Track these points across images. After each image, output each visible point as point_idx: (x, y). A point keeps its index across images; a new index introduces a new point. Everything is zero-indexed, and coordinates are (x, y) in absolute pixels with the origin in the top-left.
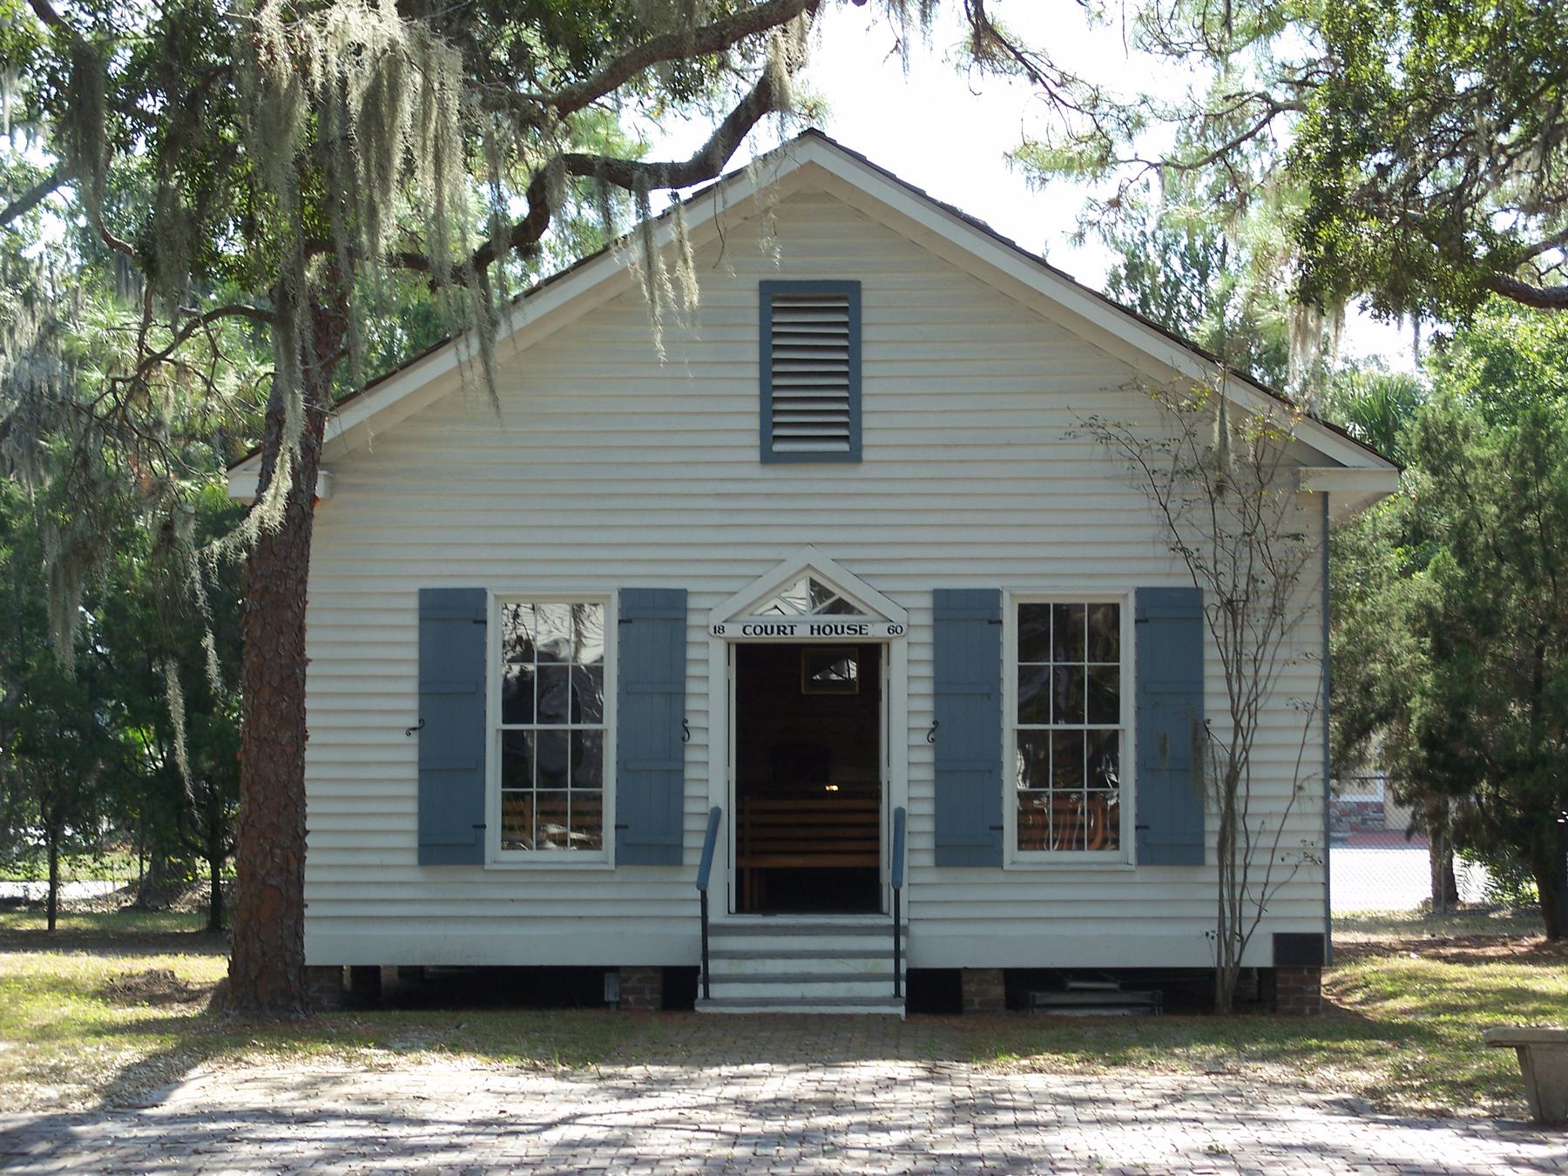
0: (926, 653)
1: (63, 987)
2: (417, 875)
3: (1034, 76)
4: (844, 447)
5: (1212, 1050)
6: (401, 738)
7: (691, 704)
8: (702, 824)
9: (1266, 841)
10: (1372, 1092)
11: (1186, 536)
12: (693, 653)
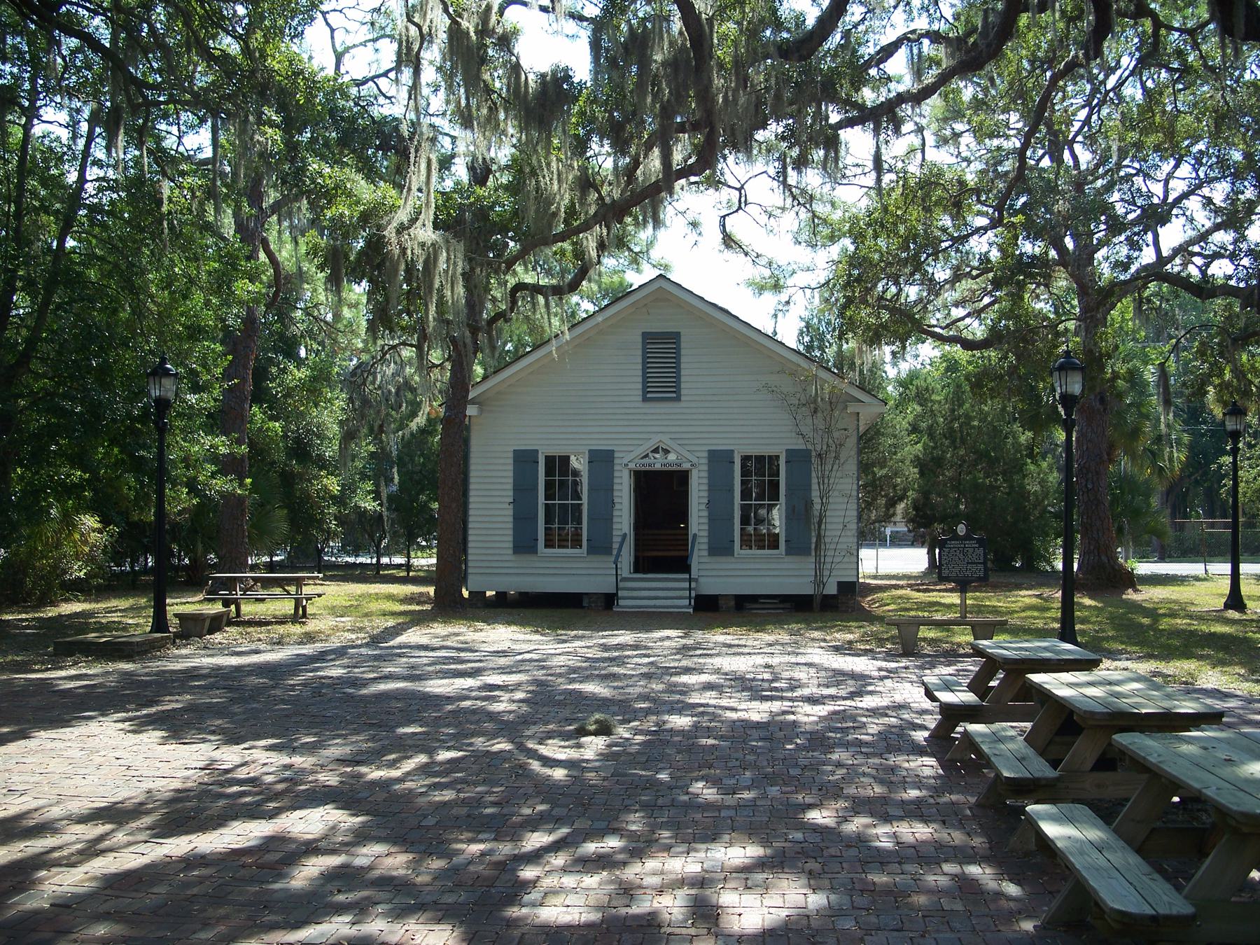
0: (705, 474)
1: (390, 597)
2: (513, 558)
3: (746, 254)
4: (674, 395)
5: (795, 626)
6: (507, 506)
7: (616, 494)
8: (619, 539)
9: (833, 546)
10: (850, 642)
11: (804, 430)
12: (616, 474)
